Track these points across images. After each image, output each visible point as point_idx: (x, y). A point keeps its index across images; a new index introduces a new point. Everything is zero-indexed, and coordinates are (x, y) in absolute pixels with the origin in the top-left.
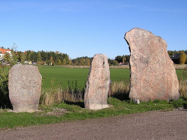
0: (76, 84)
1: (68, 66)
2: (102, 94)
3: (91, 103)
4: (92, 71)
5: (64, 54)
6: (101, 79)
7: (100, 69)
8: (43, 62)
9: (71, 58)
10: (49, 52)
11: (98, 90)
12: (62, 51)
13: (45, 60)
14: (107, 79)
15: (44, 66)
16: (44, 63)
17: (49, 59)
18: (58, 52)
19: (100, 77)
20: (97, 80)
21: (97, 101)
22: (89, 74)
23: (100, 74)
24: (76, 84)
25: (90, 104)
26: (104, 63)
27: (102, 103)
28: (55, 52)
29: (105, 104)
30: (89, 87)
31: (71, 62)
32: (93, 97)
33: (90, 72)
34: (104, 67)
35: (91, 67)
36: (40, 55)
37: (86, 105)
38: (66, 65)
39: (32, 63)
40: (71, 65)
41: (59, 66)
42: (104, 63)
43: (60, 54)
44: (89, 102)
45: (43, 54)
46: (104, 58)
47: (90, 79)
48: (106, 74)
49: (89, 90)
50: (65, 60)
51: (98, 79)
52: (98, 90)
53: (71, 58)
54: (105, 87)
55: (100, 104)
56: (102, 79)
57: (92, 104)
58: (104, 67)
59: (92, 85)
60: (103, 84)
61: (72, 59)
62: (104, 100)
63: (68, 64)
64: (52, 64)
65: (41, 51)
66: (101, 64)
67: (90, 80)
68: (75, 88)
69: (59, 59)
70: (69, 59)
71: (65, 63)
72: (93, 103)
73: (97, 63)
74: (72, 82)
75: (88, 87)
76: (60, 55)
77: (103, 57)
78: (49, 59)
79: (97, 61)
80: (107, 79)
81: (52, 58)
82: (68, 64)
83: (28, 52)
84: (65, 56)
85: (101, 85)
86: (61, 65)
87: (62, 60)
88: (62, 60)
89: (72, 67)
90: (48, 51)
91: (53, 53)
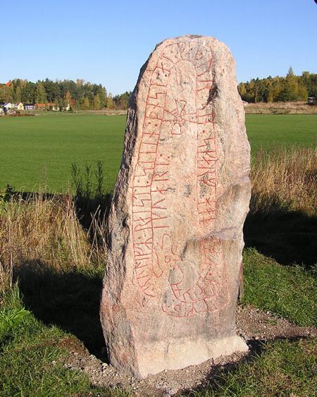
0: (100, 171)
1: (104, 111)
2: (208, 279)
3: (143, 339)
4: (144, 145)
5: (95, 85)
6: (196, 191)
7: (193, 129)
8: (49, 104)
9: (110, 94)
10: (63, 81)
11: (182, 257)
12: (92, 79)
13: (53, 101)
14: (236, 188)
15: (50, 112)
16: (51, 107)
17: (62, 96)
18: (82, 81)
19: (195, 181)
20: (173, 204)
21: (180, 325)
22: (125, 166)
23: (189, 163)
24: (100, 171)
25: (138, 346)
26: (214, 92)
27: (208, 331)
28: (76, 82)
29: (228, 333)
30: (130, 244)
31: (110, 103)
32: (154, 302)
33: (131, 152)
34: (214, 117)
35: (134, 119)
36: (41, 90)
37: (118, 349)
38: (100, 109)
39: (25, 108)
40: (112, 108)
41: (84, 112)
42: (214, 92)
43: (86, 85)
44: (131, 336)
45: (48, 86)
46: (213, 61)
47: (128, 196)
48: (229, 158)
49: (130, 261)
50: (97, 98)
51: (181, 190)
52: (182, 257)
53: (110, 94)
54: (227, 236)
55: (194, 340)
56: (204, 191)
57: (149, 346)
58: (214, 117)
59: (146, 235)
60: (211, 224)
61: (114, 96)
62: (222, 313)
63: (106, 106)
64: (68, 108)
65: (45, 81)
66: (196, 101)
67: (128, 202)
68: (100, 188)
69: (85, 96)
70: (108, 95)
71: (98, 106)
72: (154, 339)
73: (173, 92)
74: (88, 170)
75: (124, 248)
76: (86, 88)
77: (208, 56)
78: (62, 96)
79: (169, 82)
80: (236, 188)
81: (68, 95)
82: (106, 106)
83: (16, 84)
84: (97, 90)
85: (199, 230)
86: (89, 109)
87: (91, 99)
88: (91, 99)
89: (113, 112)
90: (59, 80)
91: (71, 84)
